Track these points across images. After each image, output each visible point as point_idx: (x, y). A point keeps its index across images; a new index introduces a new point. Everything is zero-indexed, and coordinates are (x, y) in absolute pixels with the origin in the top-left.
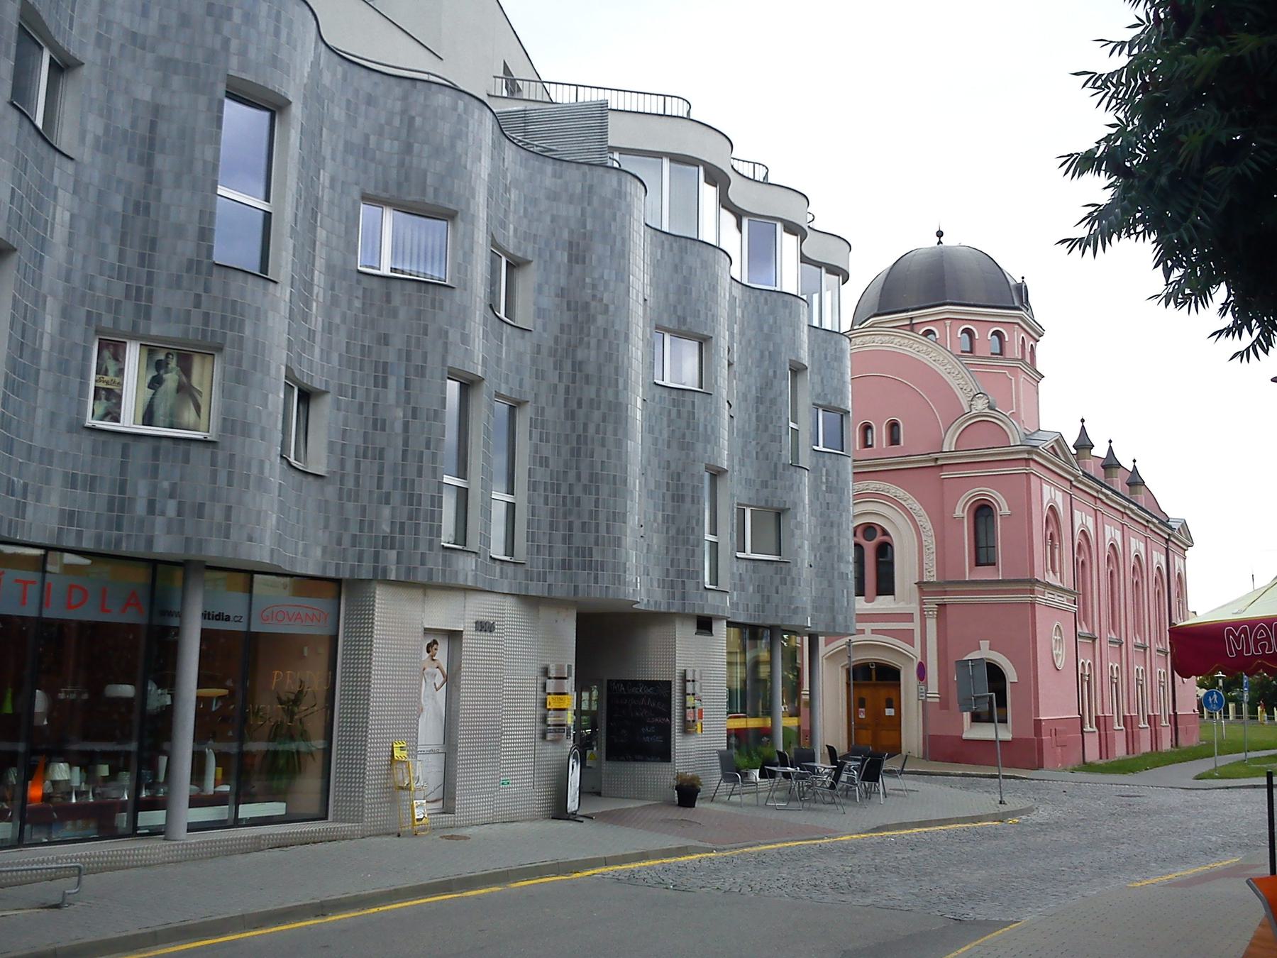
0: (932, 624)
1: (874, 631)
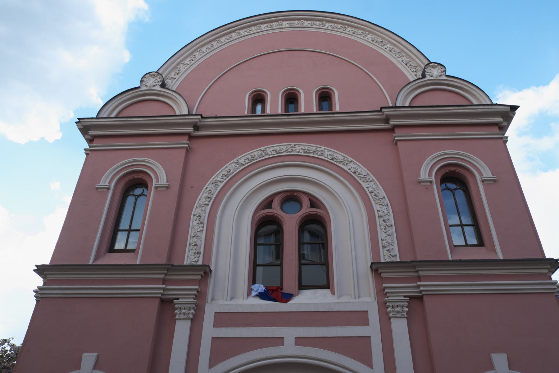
0: (400, 328)
1: (300, 341)
